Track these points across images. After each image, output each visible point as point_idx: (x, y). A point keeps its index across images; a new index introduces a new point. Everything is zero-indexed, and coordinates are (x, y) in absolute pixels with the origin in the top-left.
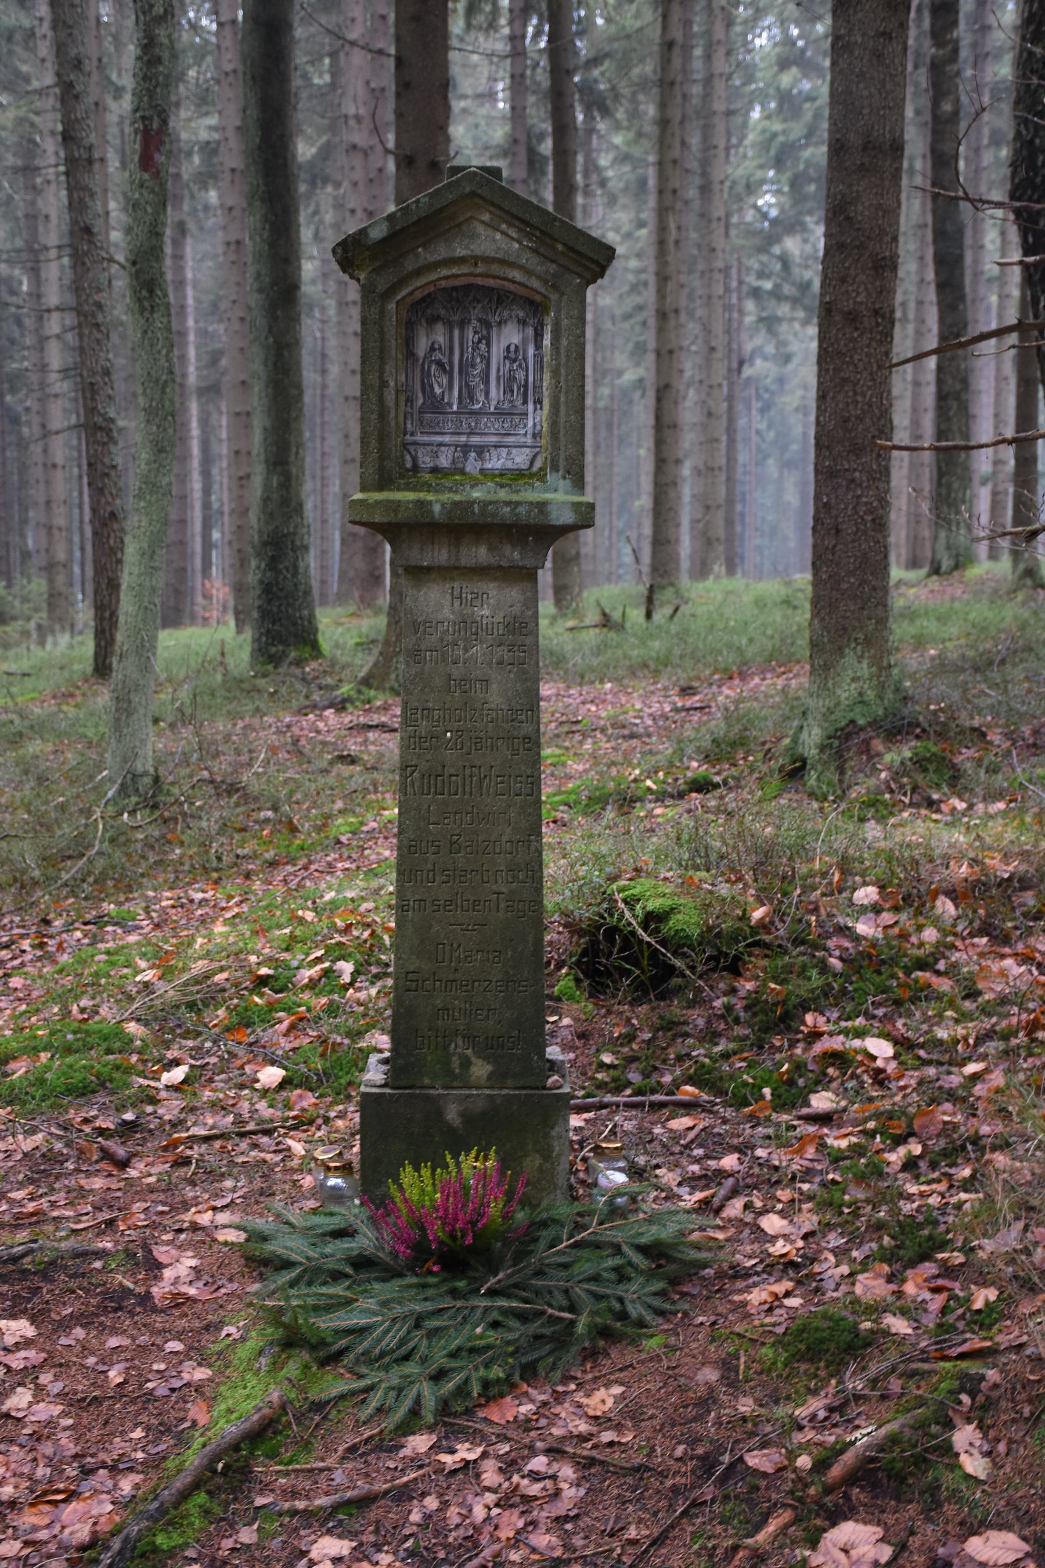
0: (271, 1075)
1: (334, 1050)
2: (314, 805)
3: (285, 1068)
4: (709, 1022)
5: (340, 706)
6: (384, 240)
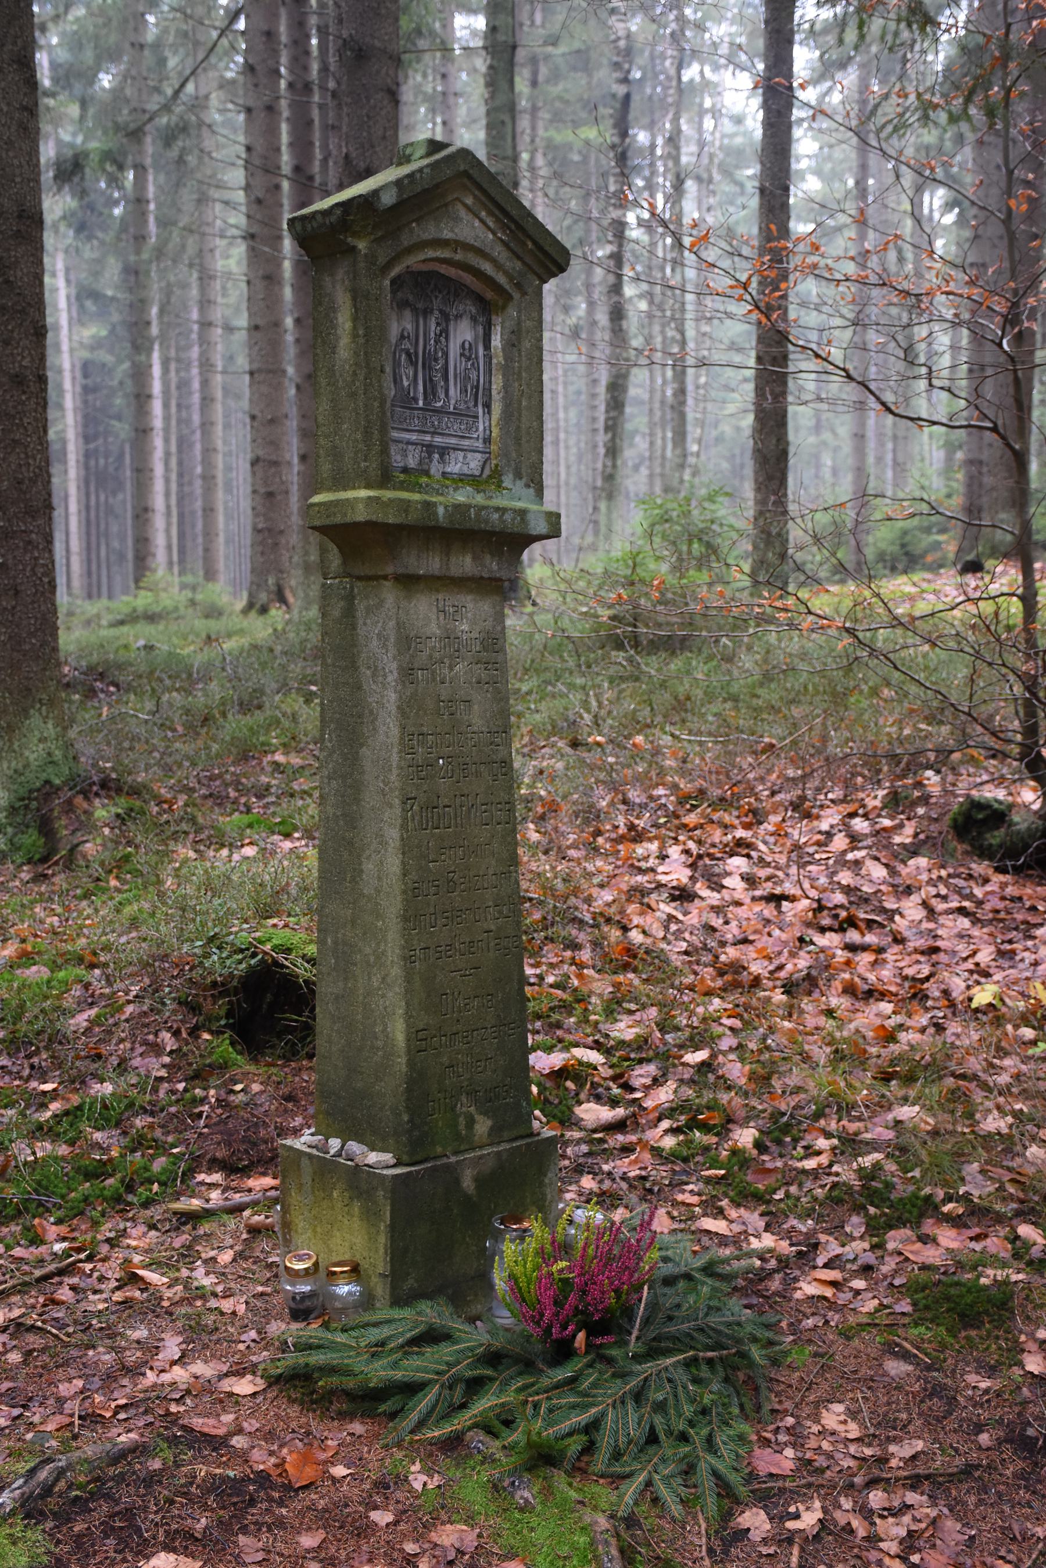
6: (393, 208)
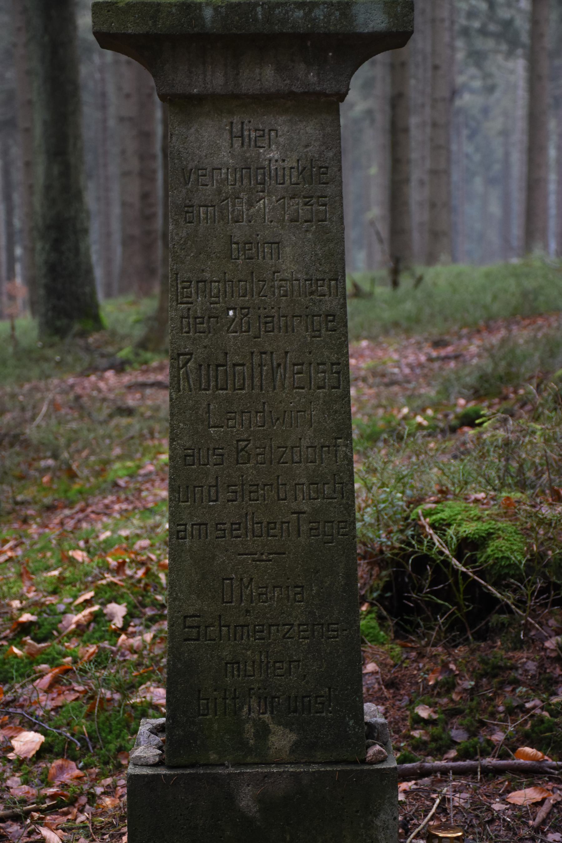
0: (28, 741)
1: (102, 709)
2: (93, 453)
3: (44, 733)
4: (541, 666)
5: (120, 368)
